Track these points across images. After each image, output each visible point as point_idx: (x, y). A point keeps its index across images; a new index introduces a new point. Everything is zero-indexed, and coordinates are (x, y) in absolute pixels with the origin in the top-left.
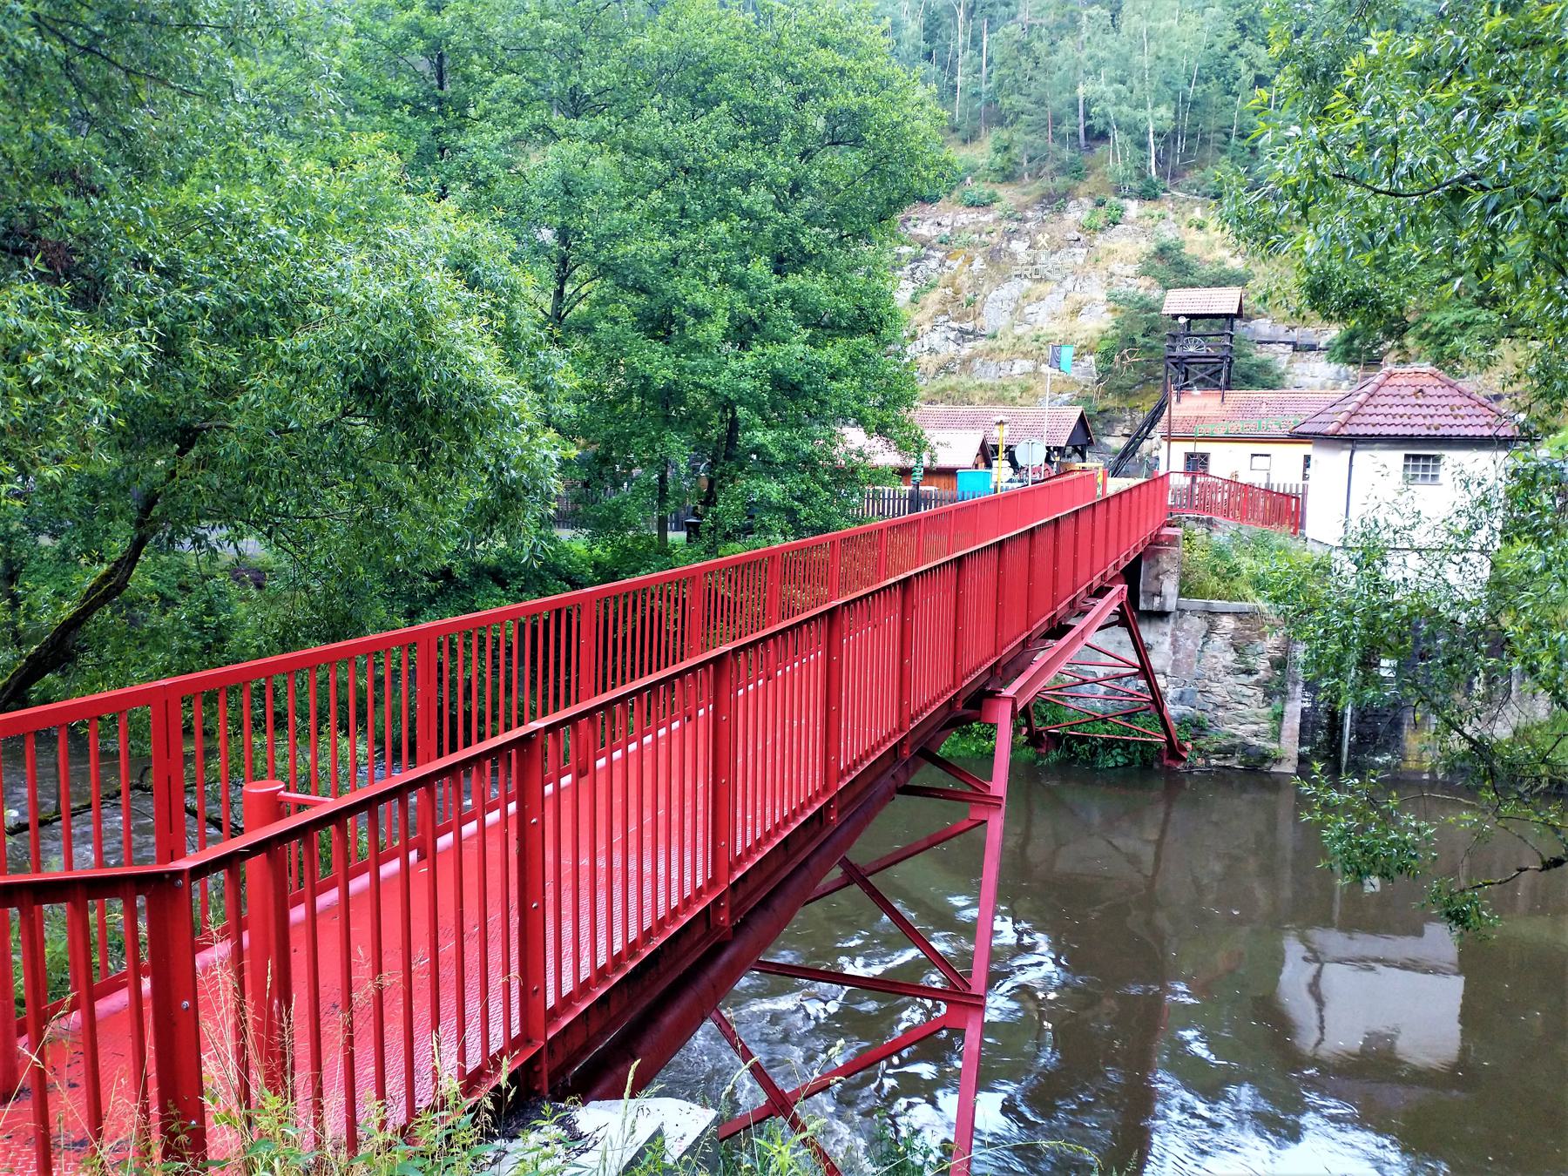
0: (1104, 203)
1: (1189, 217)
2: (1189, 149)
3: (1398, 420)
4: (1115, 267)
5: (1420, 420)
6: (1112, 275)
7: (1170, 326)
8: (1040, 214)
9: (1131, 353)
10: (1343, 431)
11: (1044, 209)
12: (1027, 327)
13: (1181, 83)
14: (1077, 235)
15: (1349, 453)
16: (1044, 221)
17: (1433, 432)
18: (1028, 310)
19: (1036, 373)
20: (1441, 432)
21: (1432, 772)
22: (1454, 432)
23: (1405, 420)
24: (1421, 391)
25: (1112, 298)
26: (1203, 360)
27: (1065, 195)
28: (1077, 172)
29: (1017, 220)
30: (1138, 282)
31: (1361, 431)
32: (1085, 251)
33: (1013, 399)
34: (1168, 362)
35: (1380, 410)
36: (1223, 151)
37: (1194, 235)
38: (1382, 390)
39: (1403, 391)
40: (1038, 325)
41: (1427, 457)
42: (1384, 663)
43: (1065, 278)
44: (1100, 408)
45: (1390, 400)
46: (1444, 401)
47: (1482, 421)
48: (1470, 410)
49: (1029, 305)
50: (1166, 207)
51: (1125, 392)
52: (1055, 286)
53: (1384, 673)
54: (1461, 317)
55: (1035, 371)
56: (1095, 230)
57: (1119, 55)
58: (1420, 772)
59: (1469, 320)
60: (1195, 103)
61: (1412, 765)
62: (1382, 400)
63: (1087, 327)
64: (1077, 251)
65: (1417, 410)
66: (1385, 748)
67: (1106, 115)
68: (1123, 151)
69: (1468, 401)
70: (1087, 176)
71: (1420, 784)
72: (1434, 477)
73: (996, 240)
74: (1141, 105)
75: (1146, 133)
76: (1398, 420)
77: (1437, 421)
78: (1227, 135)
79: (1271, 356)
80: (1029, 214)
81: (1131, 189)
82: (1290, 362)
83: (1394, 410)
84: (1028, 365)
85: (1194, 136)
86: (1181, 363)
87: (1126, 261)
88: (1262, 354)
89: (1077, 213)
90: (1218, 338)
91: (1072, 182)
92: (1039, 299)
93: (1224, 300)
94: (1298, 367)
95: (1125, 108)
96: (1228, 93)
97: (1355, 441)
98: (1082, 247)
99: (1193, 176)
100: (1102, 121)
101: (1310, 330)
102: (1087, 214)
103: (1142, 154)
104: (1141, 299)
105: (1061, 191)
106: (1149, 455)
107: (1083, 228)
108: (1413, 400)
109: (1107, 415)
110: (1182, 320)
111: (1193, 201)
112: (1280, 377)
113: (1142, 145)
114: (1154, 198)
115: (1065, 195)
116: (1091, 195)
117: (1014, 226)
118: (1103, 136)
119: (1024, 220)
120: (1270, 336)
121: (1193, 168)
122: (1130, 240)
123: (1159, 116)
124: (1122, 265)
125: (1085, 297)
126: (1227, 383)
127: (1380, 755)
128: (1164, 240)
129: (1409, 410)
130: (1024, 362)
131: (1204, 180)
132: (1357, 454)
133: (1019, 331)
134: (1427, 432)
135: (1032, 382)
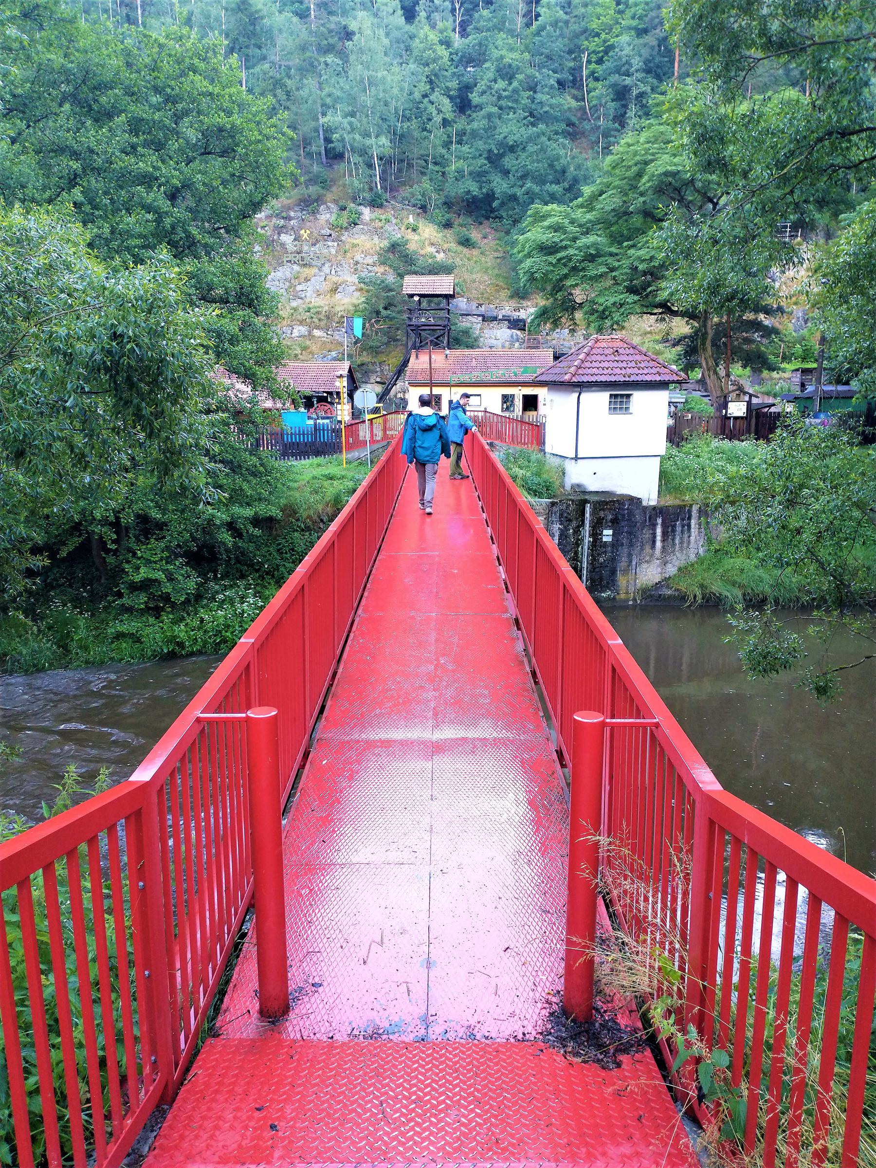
0: (345, 208)
1: (406, 222)
2: (400, 170)
3: (605, 372)
4: (358, 257)
5: (618, 371)
6: (357, 263)
7: (404, 302)
8: (299, 214)
9: (377, 322)
10: (574, 380)
11: (303, 210)
12: (300, 301)
13: (392, 118)
14: (329, 232)
15: (576, 395)
16: (303, 220)
17: (627, 379)
18: (299, 288)
19: (310, 336)
20: (633, 378)
21: (634, 600)
22: (639, 378)
23: (610, 370)
24: (617, 351)
25: (362, 280)
26: (432, 328)
27: (317, 200)
28: (325, 184)
29: (283, 218)
30: (376, 269)
31: (585, 379)
32: (336, 244)
33: (296, 355)
34: (409, 329)
35: (595, 364)
36: (423, 174)
37: (410, 236)
38: (594, 351)
39: (607, 352)
40: (308, 300)
41: (622, 396)
42: (605, 532)
43: (323, 264)
44: (359, 362)
45: (599, 358)
46: (630, 358)
47: (654, 371)
48: (646, 364)
49: (299, 284)
50: (389, 214)
51: (375, 351)
52: (317, 270)
53: (605, 539)
54: (617, 299)
55: (309, 335)
56: (342, 228)
57: (349, 95)
58: (628, 600)
59: (622, 302)
60: (402, 136)
61: (623, 596)
62: (594, 358)
63: (343, 302)
64: (330, 244)
65: (616, 364)
66: (607, 587)
67: (342, 140)
68: (357, 169)
69: (646, 358)
70: (331, 186)
71: (626, 607)
72: (627, 409)
73: (269, 233)
74: (366, 135)
75: (372, 157)
76: (605, 372)
77: (629, 371)
78: (426, 161)
79: (469, 325)
80: (292, 214)
81: (364, 199)
82: (481, 329)
83: (603, 365)
84: (304, 330)
85: (402, 161)
86: (417, 329)
87: (366, 253)
88: (464, 324)
89: (327, 216)
90: (436, 312)
91: (322, 191)
92: (307, 280)
93: (443, 284)
94: (487, 333)
95: (357, 137)
96: (425, 129)
97: (581, 386)
98: (333, 241)
99: (405, 191)
100: (341, 145)
101: (492, 306)
102: (333, 218)
103: (371, 172)
104: (383, 282)
105: (314, 197)
106: (395, 396)
107: (333, 227)
108: (612, 358)
109: (365, 367)
110: (416, 298)
111: (407, 209)
112: (476, 339)
113: (370, 166)
114: (381, 206)
115: (317, 200)
116: (335, 202)
117: (282, 222)
118: (340, 156)
119: (289, 218)
120: (467, 310)
121: (405, 185)
122: (367, 237)
123: (381, 145)
124: (363, 256)
125: (340, 279)
126: (448, 344)
127: (604, 592)
128: (394, 239)
129: (611, 364)
130: (301, 328)
131: (413, 195)
132: (583, 396)
133: (294, 304)
134: (624, 379)
135: (308, 343)
